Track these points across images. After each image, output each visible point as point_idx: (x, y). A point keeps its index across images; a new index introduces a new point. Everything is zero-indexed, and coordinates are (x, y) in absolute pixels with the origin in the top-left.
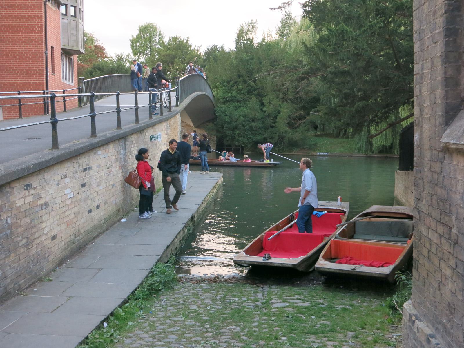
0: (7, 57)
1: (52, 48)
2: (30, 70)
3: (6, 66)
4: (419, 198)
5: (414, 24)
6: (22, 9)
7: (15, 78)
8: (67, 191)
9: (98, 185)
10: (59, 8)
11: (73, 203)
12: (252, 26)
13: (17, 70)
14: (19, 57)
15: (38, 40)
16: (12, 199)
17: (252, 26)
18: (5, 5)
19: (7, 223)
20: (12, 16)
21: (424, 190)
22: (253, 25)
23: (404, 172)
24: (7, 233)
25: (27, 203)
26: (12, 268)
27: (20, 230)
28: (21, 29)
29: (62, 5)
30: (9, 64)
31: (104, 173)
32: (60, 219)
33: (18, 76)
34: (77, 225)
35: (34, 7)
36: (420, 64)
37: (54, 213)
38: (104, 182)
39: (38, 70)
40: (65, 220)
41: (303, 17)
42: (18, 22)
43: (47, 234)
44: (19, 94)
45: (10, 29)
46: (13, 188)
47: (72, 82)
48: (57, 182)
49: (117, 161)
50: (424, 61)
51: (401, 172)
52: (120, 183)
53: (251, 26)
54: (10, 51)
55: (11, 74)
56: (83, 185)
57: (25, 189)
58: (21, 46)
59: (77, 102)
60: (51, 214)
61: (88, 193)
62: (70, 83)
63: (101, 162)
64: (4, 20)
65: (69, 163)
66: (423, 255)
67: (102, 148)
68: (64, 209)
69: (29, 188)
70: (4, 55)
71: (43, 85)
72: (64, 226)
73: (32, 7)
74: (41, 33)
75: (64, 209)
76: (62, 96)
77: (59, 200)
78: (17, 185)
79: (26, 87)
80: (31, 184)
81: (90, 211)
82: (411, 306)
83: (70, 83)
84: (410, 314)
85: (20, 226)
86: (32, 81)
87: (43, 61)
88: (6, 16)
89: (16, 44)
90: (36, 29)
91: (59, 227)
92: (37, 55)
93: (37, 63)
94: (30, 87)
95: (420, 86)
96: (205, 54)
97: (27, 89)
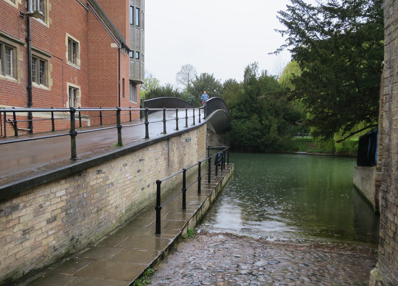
1: (123, 79)
2: (109, 94)
3: (93, 91)
4: (386, 191)
5: (384, 56)
6: (104, 54)
7: (99, 99)
8: (127, 175)
9: (149, 171)
10: (128, 53)
11: (131, 183)
12: (255, 65)
13: (100, 93)
14: (101, 85)
15: (114, 74)
16: (88, 180)
17: (255, 65)
19: (83, 196)
20: (98, 58)
21: (391, 185)
22: (256, 66)
23: (361, 167)
24: (83, 204)
25: (98, 183)
26: (86, 228)
27: (92, 202)
28: (103, 67)
29: (131, 52)
30: (95, 89)
31: (154, 162)
32: (121, 194)
33: (101, 98)
34: (133, 198)
35: (112, 52)
36: (390, 86)
37: (117, 190)
38: (153, 169)
39: (114, 94)
40: (125, 195)
41: (292, 60)
42: (101, 62)
43: (112, 204)
44: (101, 108)
45: (96, 67)
46: (89, 173)
47: (136, 102)
48: (120, 169)
49: (163, 155)
50: (393, 84)
51: (359, 167)
52: (164, 170)
53: (254, 66)
54: (97, 81)
55: (96, 96)
56: (139, 171)
57: (97, 174)
59: (139, 115)
60: (115, 190)
61: (142, 177)
62: (135, 103)
63: (151, 155)
64: (92, 61)
65: (129, 156)
66: (389, 236)
67: (152, 146)
68: (125, 187)
69: (100, 173)
70: (92, 84)
71: (117, 103)
72: (124, 199)
73: (110, 52)
74: (116, 70)
75: (125, 187)
76: (129, 110)
77: (121, 181)
78: (92, 170)
79: (106, 105)
80: (102, 170)
81: (143, 189)
82: (376, 273)
83: (135, 103)
84: (376, 280)
85: (93, 199)
86: (109, 101)
87: (117, 88)
88: (93, 58)
89: (100, 77)
90: (113, 67)
91: (121, 199)
93: (113, 89)
94: (109, 105)
95: (389, 104)
96: (224, 84)
97: (107, 106)
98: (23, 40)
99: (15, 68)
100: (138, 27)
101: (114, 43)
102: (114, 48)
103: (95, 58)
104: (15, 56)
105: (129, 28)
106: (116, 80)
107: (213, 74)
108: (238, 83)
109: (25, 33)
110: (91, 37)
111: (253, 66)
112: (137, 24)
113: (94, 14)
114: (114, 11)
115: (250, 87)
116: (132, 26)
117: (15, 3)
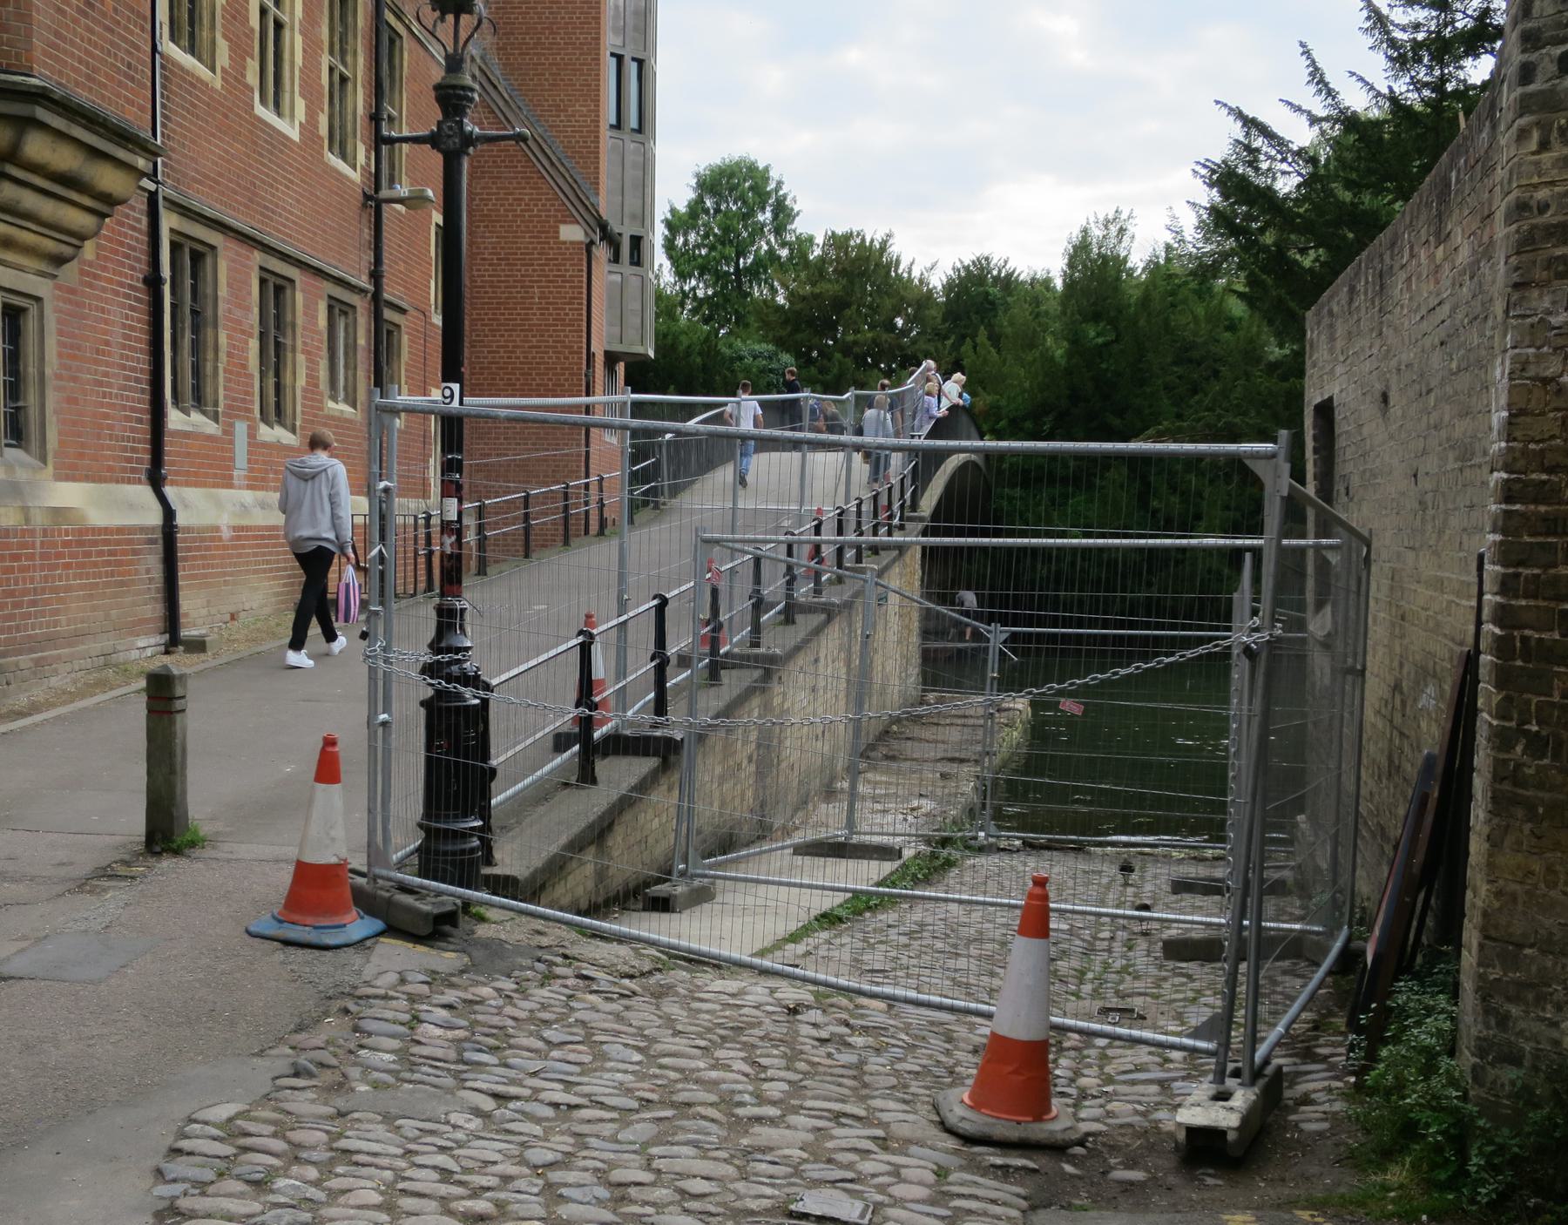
0: (492, 385)
18: (491, 254)
53: (1114, 229)
54: (501, 368)
58: (526, 358)
64: (486, 292)
90: (567, 314)
92: (567, 380)
96: (949, 287)
98: (364, 281)
99: (350, 373)
100: (638, 137)
101: (571, 222)
102: (572, 243)
103: (499, 281)
104: (351, 336)
105: (605, 134)
106: (576, 364)
107: (889, 236)
108: (1021, 278)
109: (370, 256)
110: (481, 200)
111: (1106, 227)
112: (634, 124)
113: (497, 111)
114: (553, 85)
115: (1092, 334)
116: (615, 133)
117: (213, 70)
